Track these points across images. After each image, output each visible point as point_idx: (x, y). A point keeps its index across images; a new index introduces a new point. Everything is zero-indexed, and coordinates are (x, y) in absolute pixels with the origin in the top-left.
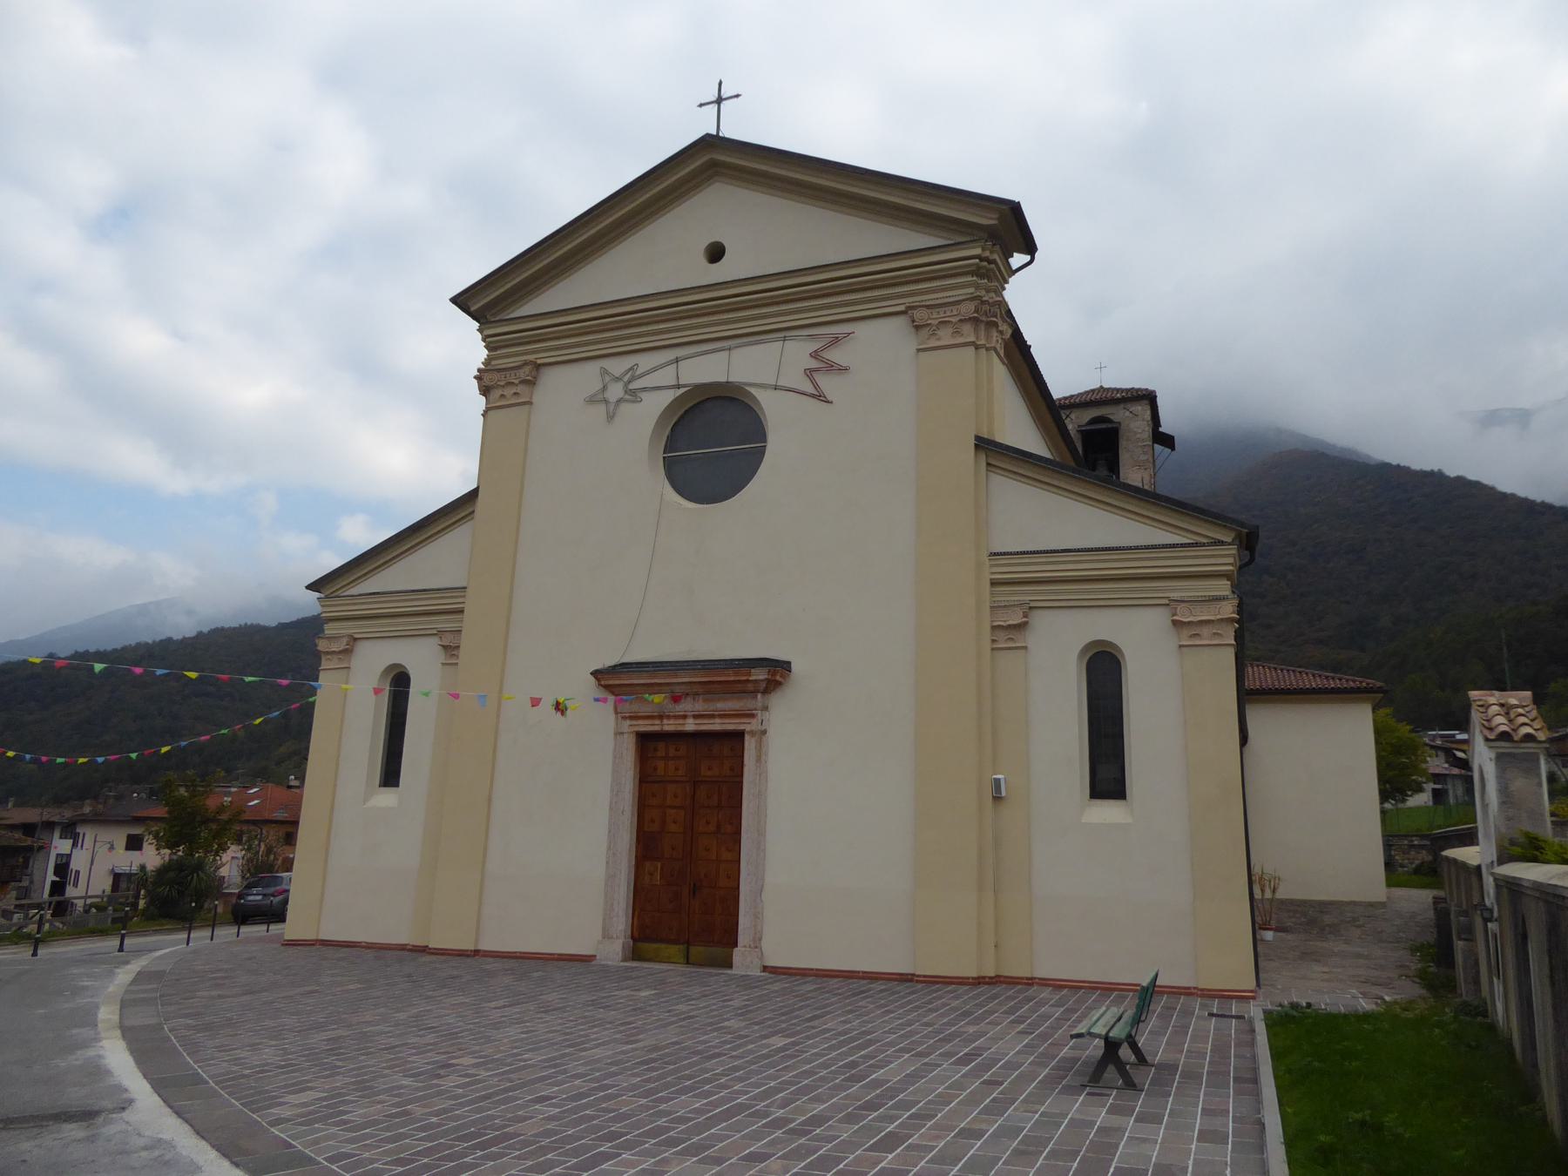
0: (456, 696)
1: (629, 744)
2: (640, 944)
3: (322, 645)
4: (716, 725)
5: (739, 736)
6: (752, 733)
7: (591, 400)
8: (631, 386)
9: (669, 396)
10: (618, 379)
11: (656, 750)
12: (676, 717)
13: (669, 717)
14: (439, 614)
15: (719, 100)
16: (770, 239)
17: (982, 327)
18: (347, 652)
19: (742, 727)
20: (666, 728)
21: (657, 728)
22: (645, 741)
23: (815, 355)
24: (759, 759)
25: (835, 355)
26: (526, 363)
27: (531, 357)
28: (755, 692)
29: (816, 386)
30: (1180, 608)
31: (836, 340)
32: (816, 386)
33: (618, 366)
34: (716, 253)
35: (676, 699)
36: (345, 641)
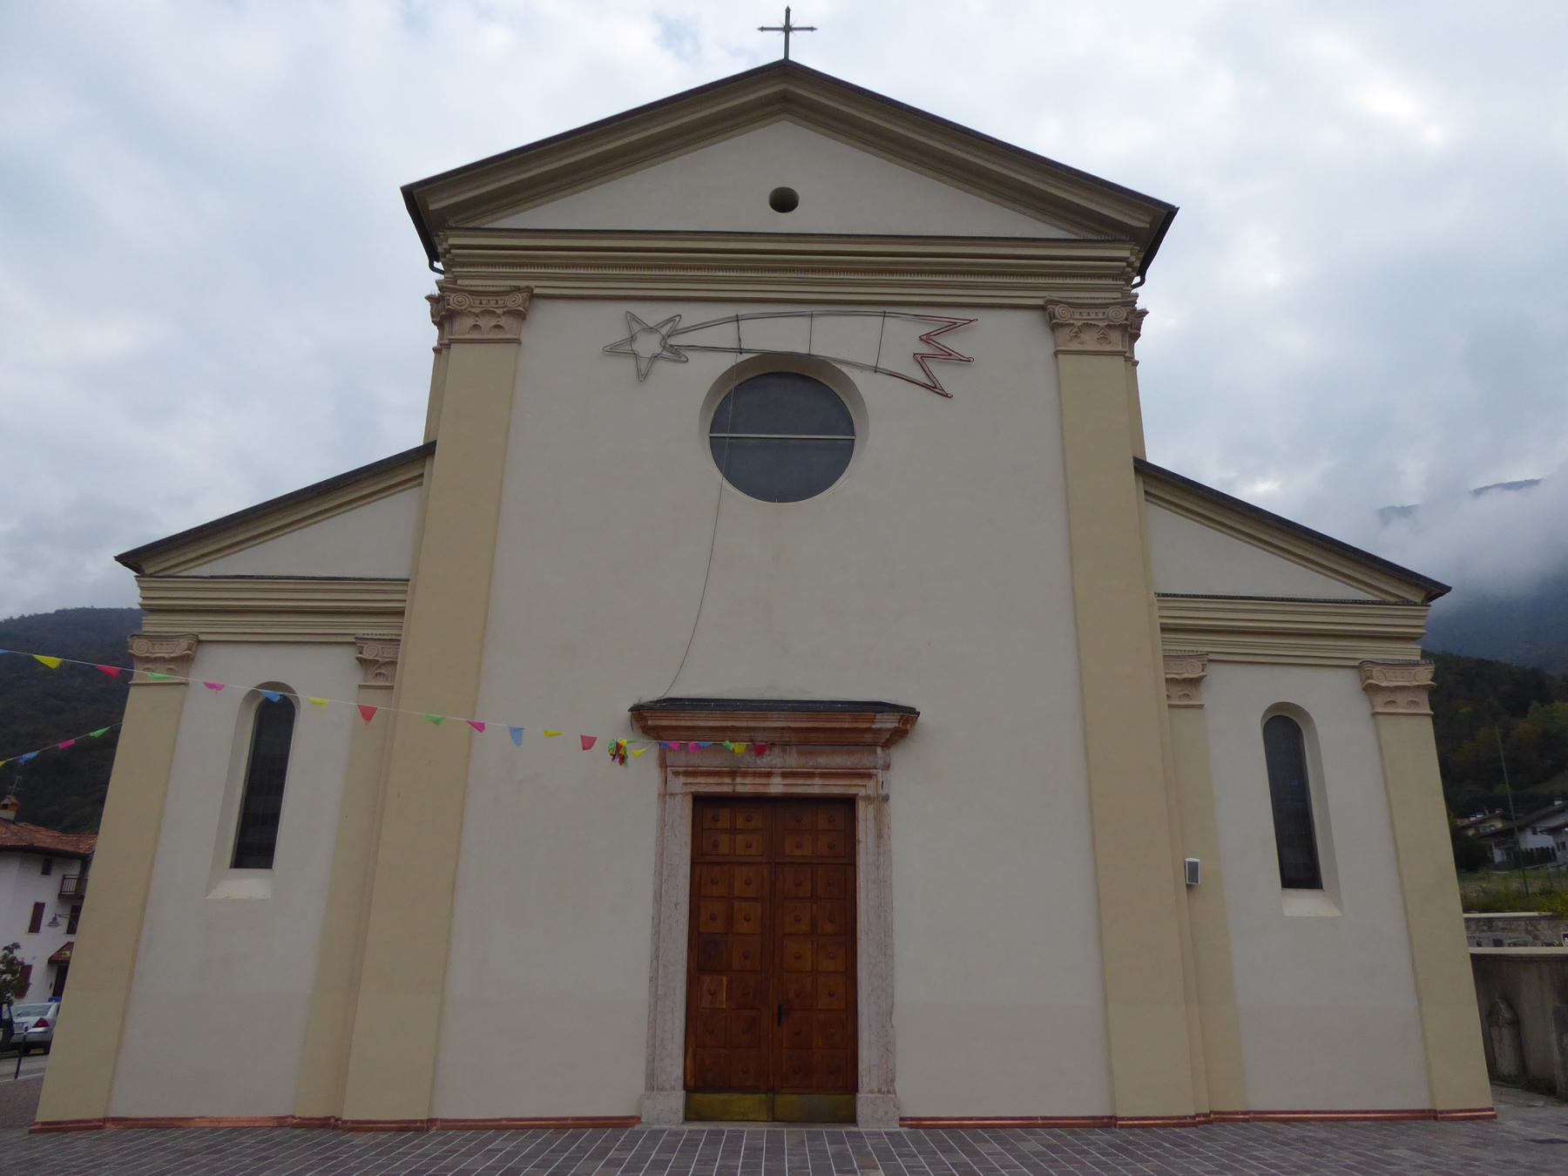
0: (480, 727)
1: (682, 812)
2: (698, 1097)
3: (139, 648)
4: (816, 787)
5: (849, 803)
6: (868, 799)
7: (613, 351)
8: (676, 341)
9: (728, 361)
11: (715, 819)
12: (756, 775)
13: (745, 774)
14: (369, 621)
15: (787, 29)
16: (851, 196)
18: (185, 660)
19: (853, 791)
20: (740, 789)
21: (726, 789)
22: (701, 802)
23: (926, 339)
24: (879, 836)
25: (950, 342)
27: (523, 284)
28: (875, 744)
29: (928, 374)
30: (1376, 670)
31: (952, 326)
32: (928, 374)
33: (653, 314)
34: (784, 201)
35: (760, 751)
36: (184, 643)
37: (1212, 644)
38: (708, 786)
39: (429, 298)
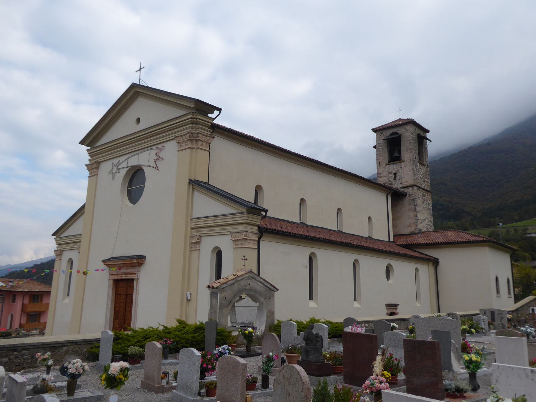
1: (111, 282)
5: (133, 280)
10: (115, 165)
16: (149, 115)
17: (194, 142)
26: (95, 162)
27: (96, 160)
33: (115, 161)
34: (138, 120)
35: (120, 269)
37: (202, 231)
38: (116, 277)
39: (86, 165)
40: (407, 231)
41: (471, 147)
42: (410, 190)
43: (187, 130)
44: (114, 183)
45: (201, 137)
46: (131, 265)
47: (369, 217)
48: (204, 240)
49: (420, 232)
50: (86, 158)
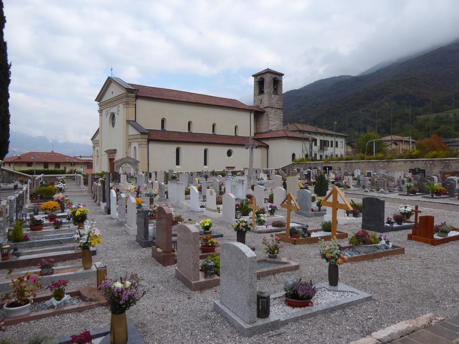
33: (107, 110)
40: (264, 131)
41: (442, 47)
42: (266, 109)
43: (124, 100)
44: (107, 119)
45: (130, 102)
46: (112, 153)
47: (245, 125)
48: (132, 144)
49: (271, 131)
50: (98, 108)
